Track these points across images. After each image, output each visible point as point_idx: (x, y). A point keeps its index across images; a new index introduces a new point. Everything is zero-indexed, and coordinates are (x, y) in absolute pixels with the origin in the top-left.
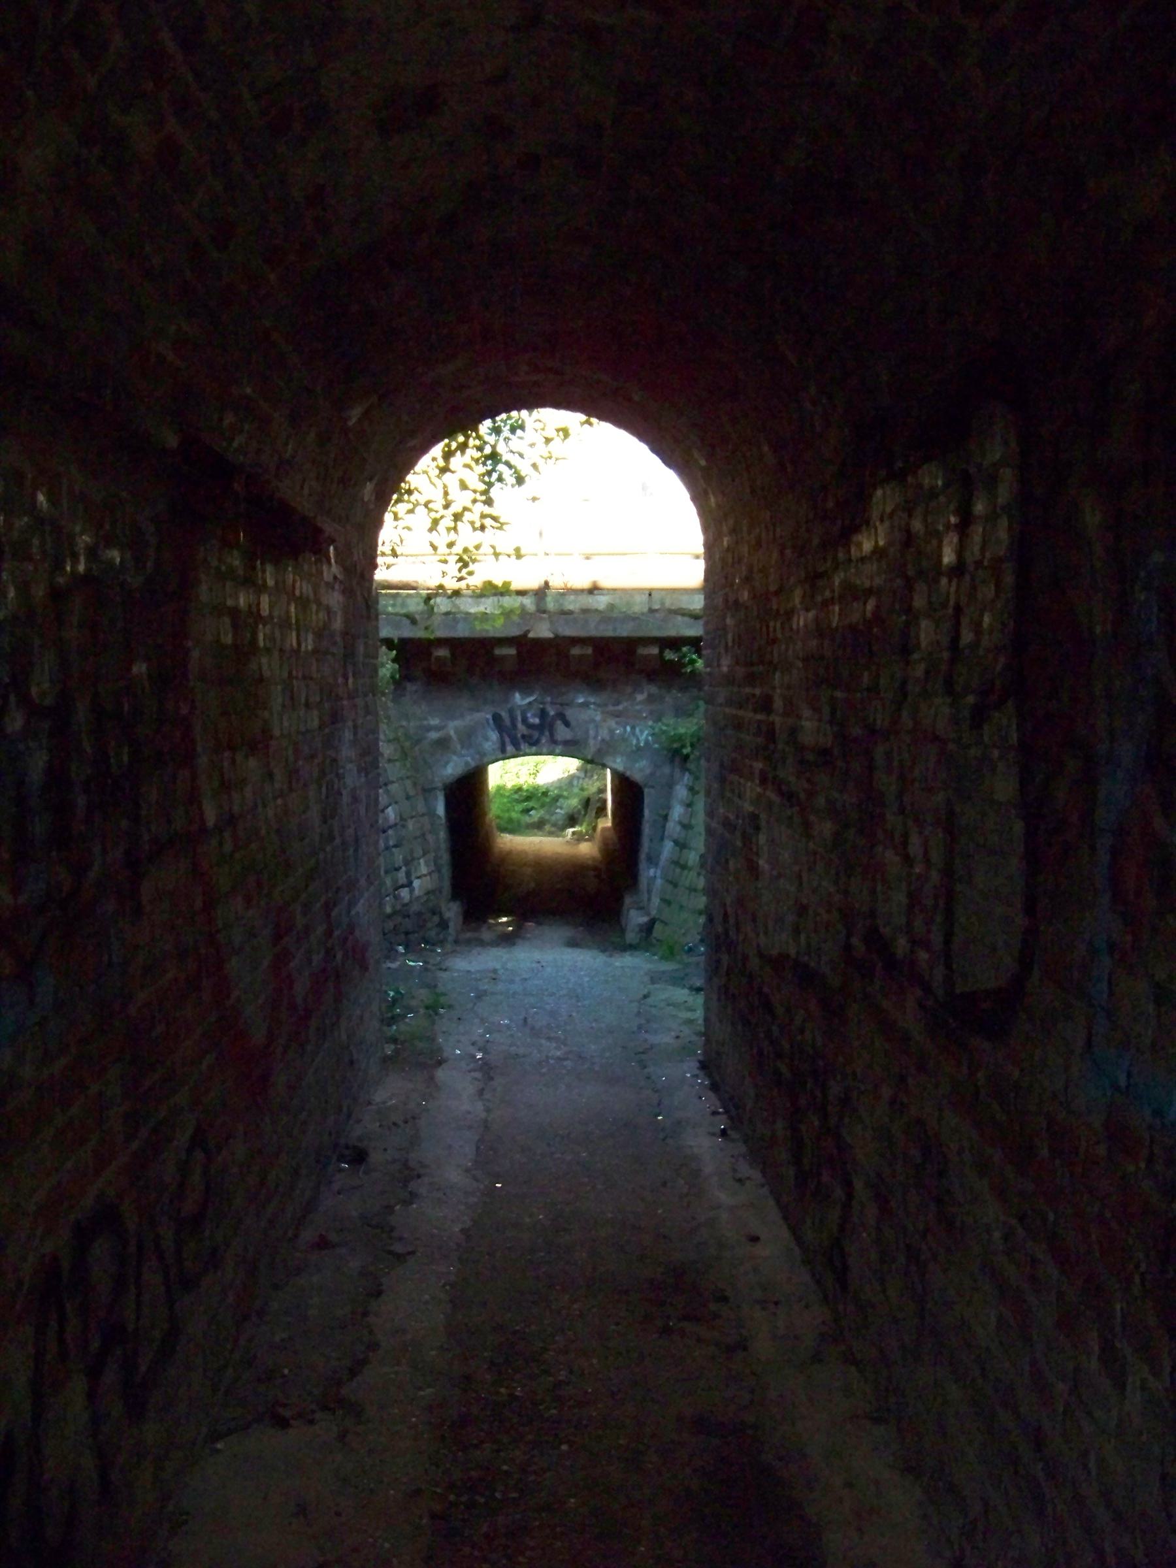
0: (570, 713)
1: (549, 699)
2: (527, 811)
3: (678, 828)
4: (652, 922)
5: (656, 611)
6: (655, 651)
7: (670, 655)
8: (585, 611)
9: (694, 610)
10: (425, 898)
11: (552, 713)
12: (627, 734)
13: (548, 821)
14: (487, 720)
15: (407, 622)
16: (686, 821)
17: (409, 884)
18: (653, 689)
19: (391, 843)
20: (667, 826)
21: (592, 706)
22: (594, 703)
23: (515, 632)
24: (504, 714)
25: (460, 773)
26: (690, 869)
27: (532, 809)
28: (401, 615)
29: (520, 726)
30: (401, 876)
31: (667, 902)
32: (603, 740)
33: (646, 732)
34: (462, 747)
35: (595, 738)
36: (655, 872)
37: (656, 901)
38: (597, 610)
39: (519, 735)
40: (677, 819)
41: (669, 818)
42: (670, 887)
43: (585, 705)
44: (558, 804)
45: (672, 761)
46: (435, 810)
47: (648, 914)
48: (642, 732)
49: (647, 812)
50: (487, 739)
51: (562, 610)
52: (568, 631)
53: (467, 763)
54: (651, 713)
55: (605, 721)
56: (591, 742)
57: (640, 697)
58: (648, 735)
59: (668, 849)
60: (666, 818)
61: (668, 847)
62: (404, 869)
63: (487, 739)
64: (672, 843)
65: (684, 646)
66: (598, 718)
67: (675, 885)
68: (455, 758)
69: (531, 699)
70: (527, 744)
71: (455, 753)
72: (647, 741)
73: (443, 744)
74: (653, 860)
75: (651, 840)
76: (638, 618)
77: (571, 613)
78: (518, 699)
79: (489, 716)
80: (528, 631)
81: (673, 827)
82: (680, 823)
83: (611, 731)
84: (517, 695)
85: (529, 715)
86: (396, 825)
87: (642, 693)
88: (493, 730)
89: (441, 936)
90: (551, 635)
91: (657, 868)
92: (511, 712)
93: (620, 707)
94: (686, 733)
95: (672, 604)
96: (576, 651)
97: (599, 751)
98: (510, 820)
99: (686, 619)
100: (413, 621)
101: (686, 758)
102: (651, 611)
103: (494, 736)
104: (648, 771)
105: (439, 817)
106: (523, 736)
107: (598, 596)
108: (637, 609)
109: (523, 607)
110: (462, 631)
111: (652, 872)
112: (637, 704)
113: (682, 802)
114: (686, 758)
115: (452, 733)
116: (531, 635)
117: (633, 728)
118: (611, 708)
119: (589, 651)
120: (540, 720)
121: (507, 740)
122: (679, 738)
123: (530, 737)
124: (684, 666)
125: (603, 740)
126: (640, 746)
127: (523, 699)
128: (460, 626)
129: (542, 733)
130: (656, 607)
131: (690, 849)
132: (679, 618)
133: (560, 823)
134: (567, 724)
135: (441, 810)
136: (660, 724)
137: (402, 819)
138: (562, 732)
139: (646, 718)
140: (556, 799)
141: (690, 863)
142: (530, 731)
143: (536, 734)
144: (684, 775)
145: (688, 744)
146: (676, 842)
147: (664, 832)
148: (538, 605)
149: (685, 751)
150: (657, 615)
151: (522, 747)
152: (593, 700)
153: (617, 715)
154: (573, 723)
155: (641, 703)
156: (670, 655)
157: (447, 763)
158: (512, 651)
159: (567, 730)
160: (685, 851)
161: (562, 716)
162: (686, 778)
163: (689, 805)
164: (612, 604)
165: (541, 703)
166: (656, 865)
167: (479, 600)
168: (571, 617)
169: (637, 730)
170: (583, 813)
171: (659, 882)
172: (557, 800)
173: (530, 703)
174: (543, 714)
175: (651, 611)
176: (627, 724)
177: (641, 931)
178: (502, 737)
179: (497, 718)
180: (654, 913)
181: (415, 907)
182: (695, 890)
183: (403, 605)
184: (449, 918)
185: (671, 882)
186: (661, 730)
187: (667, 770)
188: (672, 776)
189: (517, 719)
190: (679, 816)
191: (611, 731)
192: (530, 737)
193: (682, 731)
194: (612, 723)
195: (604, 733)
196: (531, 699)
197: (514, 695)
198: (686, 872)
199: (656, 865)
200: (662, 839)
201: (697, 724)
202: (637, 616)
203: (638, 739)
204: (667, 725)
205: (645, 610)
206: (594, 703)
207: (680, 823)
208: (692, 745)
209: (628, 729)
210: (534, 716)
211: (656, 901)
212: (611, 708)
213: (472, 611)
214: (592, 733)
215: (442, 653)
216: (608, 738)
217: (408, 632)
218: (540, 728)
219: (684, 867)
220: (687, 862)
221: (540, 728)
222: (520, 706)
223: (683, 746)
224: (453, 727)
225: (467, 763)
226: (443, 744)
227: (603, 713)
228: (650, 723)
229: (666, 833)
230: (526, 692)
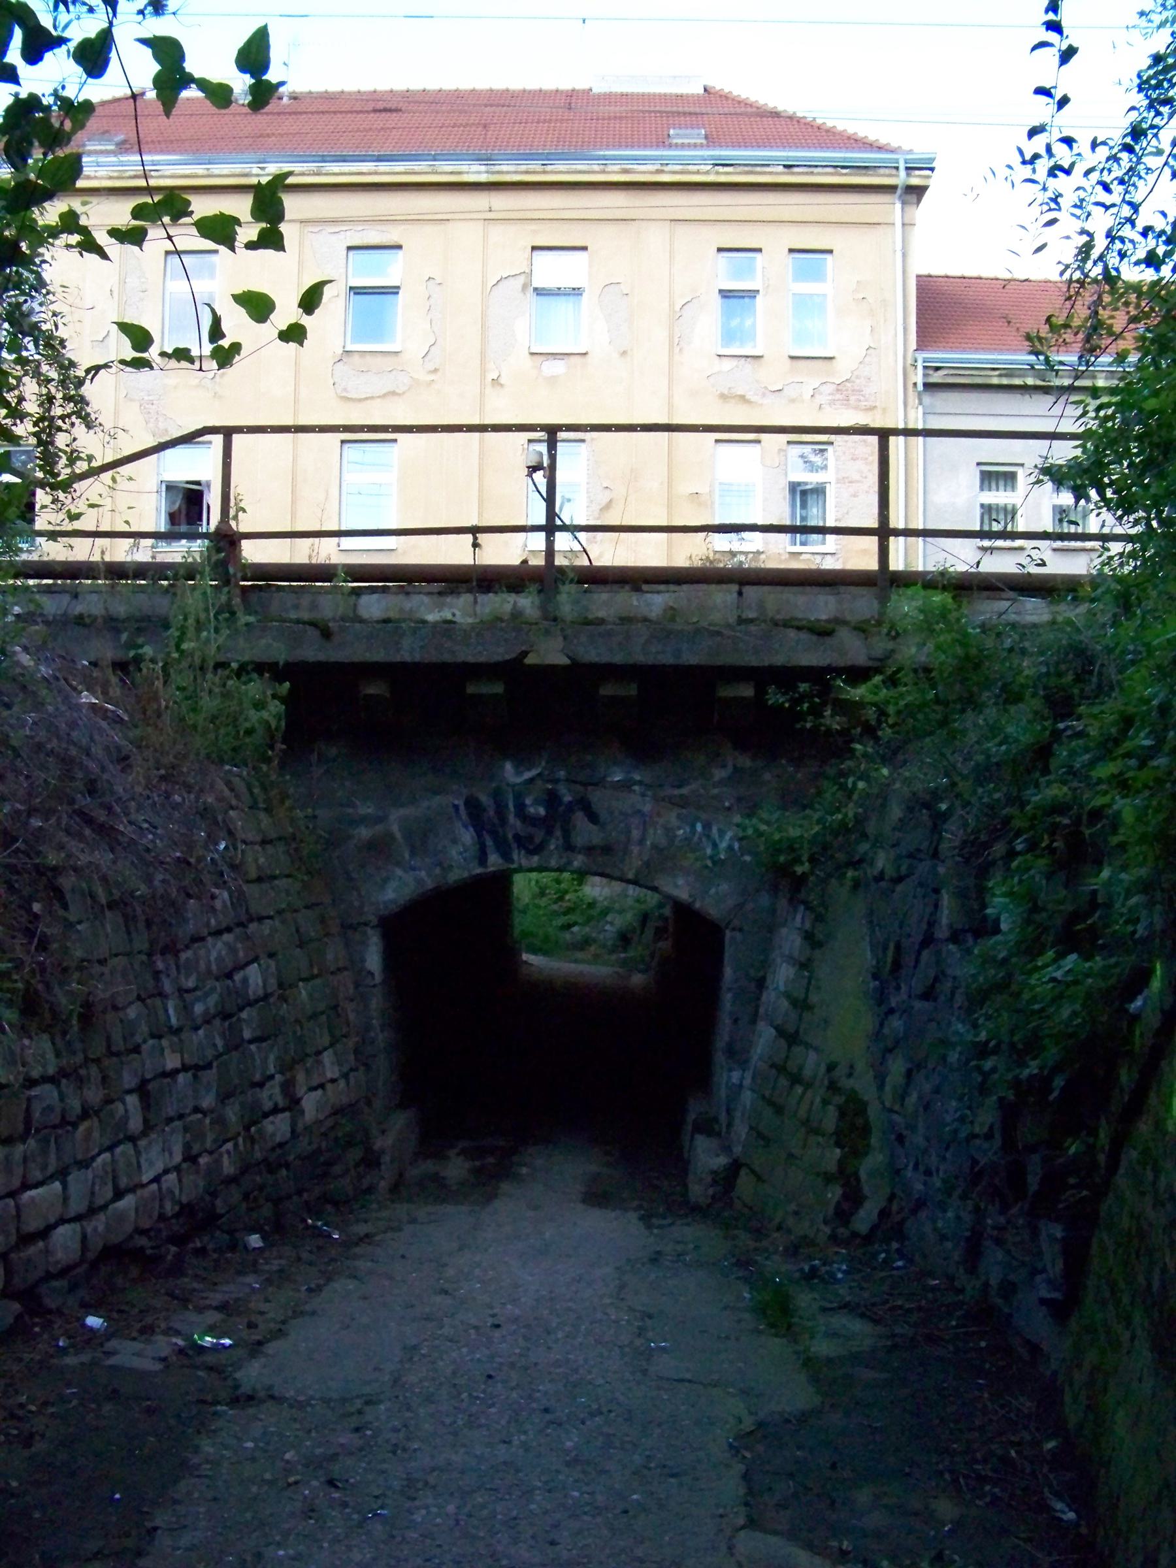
0: (596, 797)
1: (562, 774)
2: (568, 927)
3: (785, 1004)
4: (735, 1167)
5: (751, 621)
6: (747, 691)
7: (775, 697)
8: (625, 620)
9: (818, 621)
10: (329, 1123)
11: (567, 798)
12: (697, 836)
13: (595, 941)
14: (456, 807)
15: (312, 633)
16: (799, 994)
17: (293, 1104)
18: (745, 762)
19: (247, 1034)
20: (764, 998)
21: (636, 788)
22: (640, 783)
23: (499, 653)
24: (484, 799)
25: (408, 898)
26: (808, 1085)
27: (575, 924)
28: (304, 623)
29: (512, 819)
30: (271, 1094)
31: (761, 1137)
32: (655, 847)
33: (729, 834)
34: (413, 853)
35: (641, 842)
36: (742, 1078)
37: (741, 1130)
38: (646, 620)
39: (510, 836)
40: (782, 988)
41: (768, 982)
42: (768, 1112)
43: (626, 785)
44: (609, 918)
45: (775, 889)
46: (363, 960)
47: (727, 1149)
48: (722, 833)
49: (728, 972)
50: (455, 841)
51: (586, 618)
52: (593, 654)
53: (419, 882)
54: (739, 799)
55: (659, 815)
56: (635, 850)
57: (719, 774)
58: (731, 839)
59: (764, 1039)
60: (761, 983)
61: (764, 1039)
62: (278, 1077)
63: (455, 841)
64: (773, 1031)
65: (803, 682)
66: (647, 808)
67: (779, 1110)
68: (399, 872)
69: (533, 773)
70: (523, 852)
71: (398, 864)
72: (730, 848)
73: (380, 848)
74: (737, 1055)
75: (736, 1021)
76: (719, 633)
77: (601, 622)
78: (510, 772)
79: (460, 802)
80: (525, 654)
81: (774, 999)
82: (787, 995)
83: (668, 831)
84: (509, 766)
85: (528, 801)
86: (266, 997)
87: (724, 766)
88: (465, 826)
89: (365, 1183)
90: (564, 661)
91: (744, 1070)
92: (497, 795)
93: (685, 791)
94: (802, 837)
95: (778, 612)
96: (607, 690)
97: (647, 864)
98: (547, 938)
99: (804, 636)
100: (326, 634)
101: (799, 882)
102: (741, 621)
103: (467, 836)
104: (730, 902)
105: (371, 974)
106: (517, 837)
107: (649, 595)
108: (716, 617)
109: (516, 614)
110: (408, 651)
111: (735, 1076)
112: (714, 786)
113: (791, 960)
114: (799, 882)
115: (395, 829)
116: (530, 660)
117: (707, 826)
118: (669, 791)
119: (632, 690)
120: (547, 809)
121: (489, 842)
122: (791, 847)
123: (531, 838)
124: (801, 717)
125: (655, 847)
126: (167, 215)
127: (518, 773)
128: (406, 643)
129: (550, 832)
130: (751, 615)
131: (808, 1046)
132: (792, 634)
133: (609, 943)
134: (593, 817)
135: (373, 960)
136: (755, 821)
137: (281, 985)
138: (584, 831)
139: (729, 809)
140: (605, 912)
141: (807, 1073)
142: (531, 830)
143: (539, 836)
144: (795, 911)
145: (805, 858)
146: (781, 1032)
147: (757, 1007)
148: (543, 608)
149: (799, 870)
150: (752, 628)
151: (515, 857)
152: (638, 778)
153: (682, 803)
154: (603, 815)
155: (721, 782)
156: (775, 697)
157: (386, 880)
158: (498, 688)
159: (592, 827)
160: (797, 1050)
161: (586, 806)
162: (799, 917)
163: (804, 965)
164: (672, 608)
165: (549, 781)
166: (743, 1064)
167: (442, 599)
168: (602, 628)
169: (715, 830)
170: (638, 932)
171: (747, 1097)
172: (607, 914)
173: (531, 780)
174: (552, 799)
175: (741, 621)
176: (697, 819)
177: (715, 1182)
178: (479, 836)
179: (473, 806)
180: (738, 1150)
181: (304, 1145)
182: (816, 1132)
183: (314, 606)
184: (382, 1151)
185: (771, 1103)
186: (756, 830)
187: (765, 900)
188: (773, 911)
189: (507, 805)
190: (785, 984)
191: (668, 831)
192: (531, 838)
193: (794, 832)
194: (672, 817)
195: (655, 836)
196: (533, 773)
197: (502, 768)
198: (799, 1090)
199: (743, 1064)
200: (754, 1021)
201: (818, 822)
202: (716, 629)
203: (715, 845)
204: (768, 823)
205: (732, 620)
206: (640, 783)
207: (787, 995)
208: (812, 860)
209: (699, 827)
210: (537, 802)
211: (741, 1130)
212: (669, 791)
213: (431, 618)
214: (636, 834)
215: (374, 689)
216: (663, 842)
217: (312, 651)
218: (546, 824)
219: (796, 1079)
220: (801, 1068)
221: (546, 824)
222: (514, 785)
223: (798, 860)
224: (396, 820)
225: (419, 882)
226: (380, 848)
227: (655, 799)
228: (737, 819)
229: (762, 1010)
230: (521, 763)
